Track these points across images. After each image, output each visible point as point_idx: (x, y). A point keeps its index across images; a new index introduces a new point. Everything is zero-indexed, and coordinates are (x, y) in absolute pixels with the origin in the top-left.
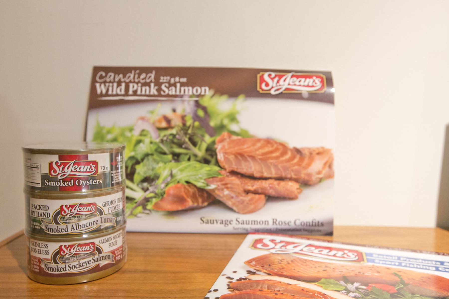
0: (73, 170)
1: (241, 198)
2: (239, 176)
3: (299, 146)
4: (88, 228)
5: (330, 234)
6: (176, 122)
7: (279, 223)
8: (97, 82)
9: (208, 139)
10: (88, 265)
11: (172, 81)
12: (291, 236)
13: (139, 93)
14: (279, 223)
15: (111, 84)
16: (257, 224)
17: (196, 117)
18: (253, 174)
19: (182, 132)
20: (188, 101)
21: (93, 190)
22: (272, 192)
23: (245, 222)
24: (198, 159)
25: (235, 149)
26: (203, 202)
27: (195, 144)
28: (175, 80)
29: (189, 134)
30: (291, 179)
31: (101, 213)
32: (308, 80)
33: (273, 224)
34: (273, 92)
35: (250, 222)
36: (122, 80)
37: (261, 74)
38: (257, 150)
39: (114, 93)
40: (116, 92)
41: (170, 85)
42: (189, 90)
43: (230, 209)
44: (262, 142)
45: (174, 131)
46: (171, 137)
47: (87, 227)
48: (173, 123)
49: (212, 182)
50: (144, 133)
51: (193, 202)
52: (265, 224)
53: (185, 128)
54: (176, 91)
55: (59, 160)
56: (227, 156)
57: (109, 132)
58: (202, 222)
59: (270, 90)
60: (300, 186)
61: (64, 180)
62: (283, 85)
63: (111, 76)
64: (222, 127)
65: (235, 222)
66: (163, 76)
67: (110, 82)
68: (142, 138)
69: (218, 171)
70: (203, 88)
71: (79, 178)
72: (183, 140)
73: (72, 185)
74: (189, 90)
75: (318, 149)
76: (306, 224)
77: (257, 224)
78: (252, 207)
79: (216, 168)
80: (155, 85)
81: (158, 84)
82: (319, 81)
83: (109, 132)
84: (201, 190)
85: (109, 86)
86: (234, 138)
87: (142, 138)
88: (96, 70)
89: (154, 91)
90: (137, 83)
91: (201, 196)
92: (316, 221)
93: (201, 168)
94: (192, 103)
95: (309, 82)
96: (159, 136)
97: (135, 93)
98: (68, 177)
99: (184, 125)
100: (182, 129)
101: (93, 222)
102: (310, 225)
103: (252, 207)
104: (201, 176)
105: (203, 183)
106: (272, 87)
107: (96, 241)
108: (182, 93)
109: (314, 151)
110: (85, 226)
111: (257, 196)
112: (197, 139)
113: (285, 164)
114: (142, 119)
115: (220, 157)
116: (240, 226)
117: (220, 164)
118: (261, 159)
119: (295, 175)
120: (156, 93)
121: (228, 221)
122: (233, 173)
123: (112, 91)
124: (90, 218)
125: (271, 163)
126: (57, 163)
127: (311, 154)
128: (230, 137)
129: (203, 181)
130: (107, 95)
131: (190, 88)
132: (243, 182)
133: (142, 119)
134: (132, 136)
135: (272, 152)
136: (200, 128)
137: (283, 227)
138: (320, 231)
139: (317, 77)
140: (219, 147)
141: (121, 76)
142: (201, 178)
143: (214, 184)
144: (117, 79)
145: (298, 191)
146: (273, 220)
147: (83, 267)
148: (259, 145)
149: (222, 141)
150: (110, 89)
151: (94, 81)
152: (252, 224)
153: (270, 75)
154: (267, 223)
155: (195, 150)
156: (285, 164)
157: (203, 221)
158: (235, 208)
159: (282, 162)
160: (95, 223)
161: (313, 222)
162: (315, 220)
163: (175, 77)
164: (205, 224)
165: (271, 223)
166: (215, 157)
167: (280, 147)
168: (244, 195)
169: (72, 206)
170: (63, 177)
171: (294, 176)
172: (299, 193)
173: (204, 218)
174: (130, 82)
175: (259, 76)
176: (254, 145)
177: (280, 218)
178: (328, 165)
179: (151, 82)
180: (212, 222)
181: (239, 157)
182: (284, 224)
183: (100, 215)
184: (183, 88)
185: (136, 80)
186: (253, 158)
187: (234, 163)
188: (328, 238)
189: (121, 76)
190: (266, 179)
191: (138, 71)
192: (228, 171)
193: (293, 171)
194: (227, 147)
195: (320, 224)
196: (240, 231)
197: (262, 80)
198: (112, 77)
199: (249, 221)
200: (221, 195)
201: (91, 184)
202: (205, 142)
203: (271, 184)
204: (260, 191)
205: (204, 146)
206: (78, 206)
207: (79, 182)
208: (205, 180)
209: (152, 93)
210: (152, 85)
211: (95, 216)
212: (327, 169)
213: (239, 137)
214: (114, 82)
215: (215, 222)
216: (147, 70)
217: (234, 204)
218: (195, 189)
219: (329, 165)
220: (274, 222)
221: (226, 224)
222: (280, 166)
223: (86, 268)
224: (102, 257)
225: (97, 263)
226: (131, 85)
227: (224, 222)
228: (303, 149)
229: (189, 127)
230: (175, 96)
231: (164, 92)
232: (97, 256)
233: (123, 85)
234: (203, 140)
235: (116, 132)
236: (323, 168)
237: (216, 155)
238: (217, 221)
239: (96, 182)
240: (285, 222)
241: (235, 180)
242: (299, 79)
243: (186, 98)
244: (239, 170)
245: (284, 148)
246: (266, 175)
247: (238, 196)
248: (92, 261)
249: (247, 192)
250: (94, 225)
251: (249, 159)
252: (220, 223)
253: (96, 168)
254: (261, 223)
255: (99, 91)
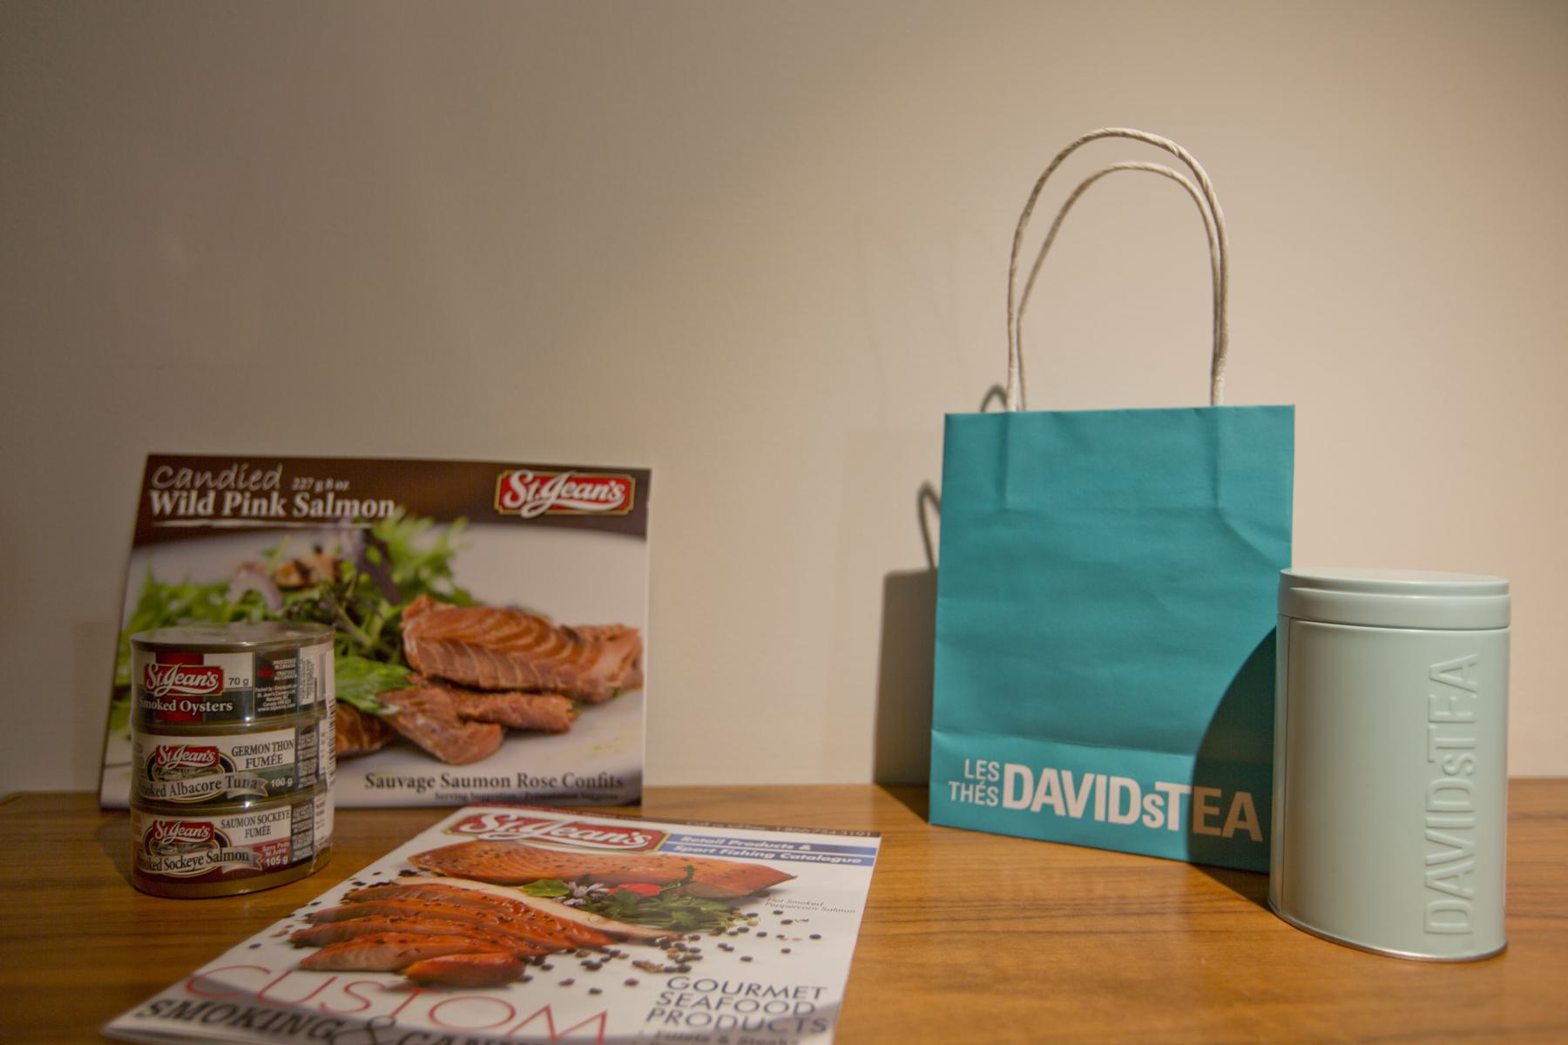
0: (180, 834)
1: (453, 731)
2: (449, 686)
3: (572, 622)
4: (200, 793)
5: (636, 803)
6: (322, 573)
7: (531, 784)
8: (154, 489)
9: (386, 610)
10: (198, 866)
11: (319, 487)
12: (548, 808)
13: (245, 511)
14: (531, 784)
15: (185, 494)
16: (486, 785)
17: (364, 564)
18: (477, 682)
19: (333, 595)
20: (350, 531)
21: (263, 719)
22: (515, 719)
23: (460, 783)
24: (364, 651)
25: (443, 631)
26: (372, 742)
27: (358, 620)
28: (324, 486)
29: (348, 601)
30: (555, 691)
31: (228, 767)
32: (598, 488)
33: (519, 785)
34: (525, 513)
35: (472, 783)
36: (211, 484)
37: (505, 474)
38: (486, 632)
39: (191, 511)
40: (196, 509)
41: (314, 496)
42: (352, 507)
43: (431, 757)
44: (498, 616)
45: (315, 594)
46: (308, 607)
47: (198, 791)
48: (314, 577)
49: (392, 700)
50: (252, 597)
51: (351, 742)
52: (503, 785)
53: (338, 586)
54: (325, 509)
55: (158, 662)
56: (423, 645)
57: (174, 596)
58: (369, 784)
59: (519, 508)
60: (575, 706)
61: (165, 699)
62: (548, 498)
63: (184, 476)
64: (416, 585)
65: (439, 781)
66: (300, 477)
67: (182, 488)
68: (246, 608)
69: (405, 678)
70: (383, 504)
71: (187, 698)
72: (333, 612)
73: (175, 709)
74: (353, 508)
75: (611, 628)
76: (586, 783)
77: (486, 785)
78: (475, 749)
79: (401, 671)
80: (280, 497)
81: (288, 494)
82: (620, 490)
83: (174, 596)
84: (368, 717)
85: (179, 498)
86: (441, 607)
87: (246, 608)
88: (154, 461)
89: (277, 508)
90: (242, 492)
91: (369, 730)
92: (608, 777)
93: (370, 671)
94: (357, 534)
95: (600, 493)
96: (283, 604)
97: (236, 512)
98: (169, 694)
99: (338, 579)
100: (333, 589)
101: (211, 783)
102: (594, 786)
103: (475, 749)
104: (367, 687)
105: (373, 701)
106: (525, 503)
107: (216, 821)
108: (338, 512)
109: (603, 632)
110: (193, 789)
111: (485, 728)
112: (363, 611)
113: (544, 661)
114: (250, 567)
115: (410, 646)
116: (450, 790)
117: (410, 662)
118: (495, 651)
119: (564, 682)
120: (282, 512)
121: (424, 780)
122: (438, 680)
123: (187, 507)
124: (203, 776)
125: (515, 659)
126: (154, 667)
127: (597, 639)
128: (431, 606)
129: (372, 697)
130: (174, 515)
131: (356, 503)
132: (458, 699)
133: (250, 567)
134: (226, 604)
135: (517, 636)
136: (370, 587)
137: (540, 790)
138: (615, 797)
139: (618, 481)
140: (408, 626)
141: (208, 475)
142: (368, 692)
143: (394, 704)
144: (198, 483)
145: (570, 715)
146: (519, 776)
147: (188, 869)
148: (490, 621)
149: (415, 613)
150: (183, 503)
151: (147, 487)
152: (475, 785)
153: (522, 478)
154: (506, 783)
155: (359, 633)
156: (544, 661)
157: (372, 783)
158: (439, 754)
159: (538, 656)
160: (214, 785)
161: (600, 779)
162: (605, 773)
163: (324, 480)
164: (375, 789)
165: (514, 782)
166: (399, 647)
167: (535, 626)
168: (457, 724)
169: (174, 749)
170: (161, 694)
171: (561, 686)
172: (572, 720)
173: (373, 775)
174: (228, 488)
175: (500, 478)
176: (481, 621)
177: (532, 774)
178: (631, 660)
179: (273, 488)
180: (390, 784)
181: (450, 647)
182: (541, 783)
183: (227, 771)
184: (339, 504)
185: (241, 485)
186: (478, 648)
187: (438, 659)
188: (631, 811)
189: (208, 475)
190: (504, 691)
191: (245, 466)
192: (425, 675)
193: (559, 674)
194: (424, 626)
195: (615, 783)
196: (450, 801)
197: (506, 487)
198: (188, 478)
199: (469, 781)
200: (411, 726)
201: (208, 710)
202: (380, 616)
203: (514, 702)
204: (491, 716)
205: (378, 624)
206: (182, 752)
207: (185, 706)
208: (377, 695)
209: (273, 512)
210: (275, 496)
211: (215, 772)
212: (628, 669)
213: (451, 606)
214: (192, 487)
215: (397, 784)
216: (265, 464)
217: (437, 745)
218: (357, 716)
219: (635, 663)
220: (522, 779)
221: (419, 786)
222: (532, 665)
223: (194, 870)
224: (229, 854)
225: (217, 865)
226: (229, 496)
227: (416, 783)
228: (581, 628)
229: (348, 585)
230: (323, 519)
231: (300, 510)
232: (216, 851)
233: (212, 495)
234: (375, 612)
235: (190, 595)
236: (621, 668)
237: (402, 642)
238: (402, 780)
239: (219, 708)
240: (543, 781)
241: (439, 695)
242: (581, 487)
243: (345, 524)
244: (449, 675)
245: (541, 626)
246: (503, 683)
247: (446, 724)
248: (206, 858)
249: (465, 719)
250: (211, 789)
251: (470, 651)
252: (409, 786)
253: (220, 680)
254: (494, 783)
255: (157, 508)
